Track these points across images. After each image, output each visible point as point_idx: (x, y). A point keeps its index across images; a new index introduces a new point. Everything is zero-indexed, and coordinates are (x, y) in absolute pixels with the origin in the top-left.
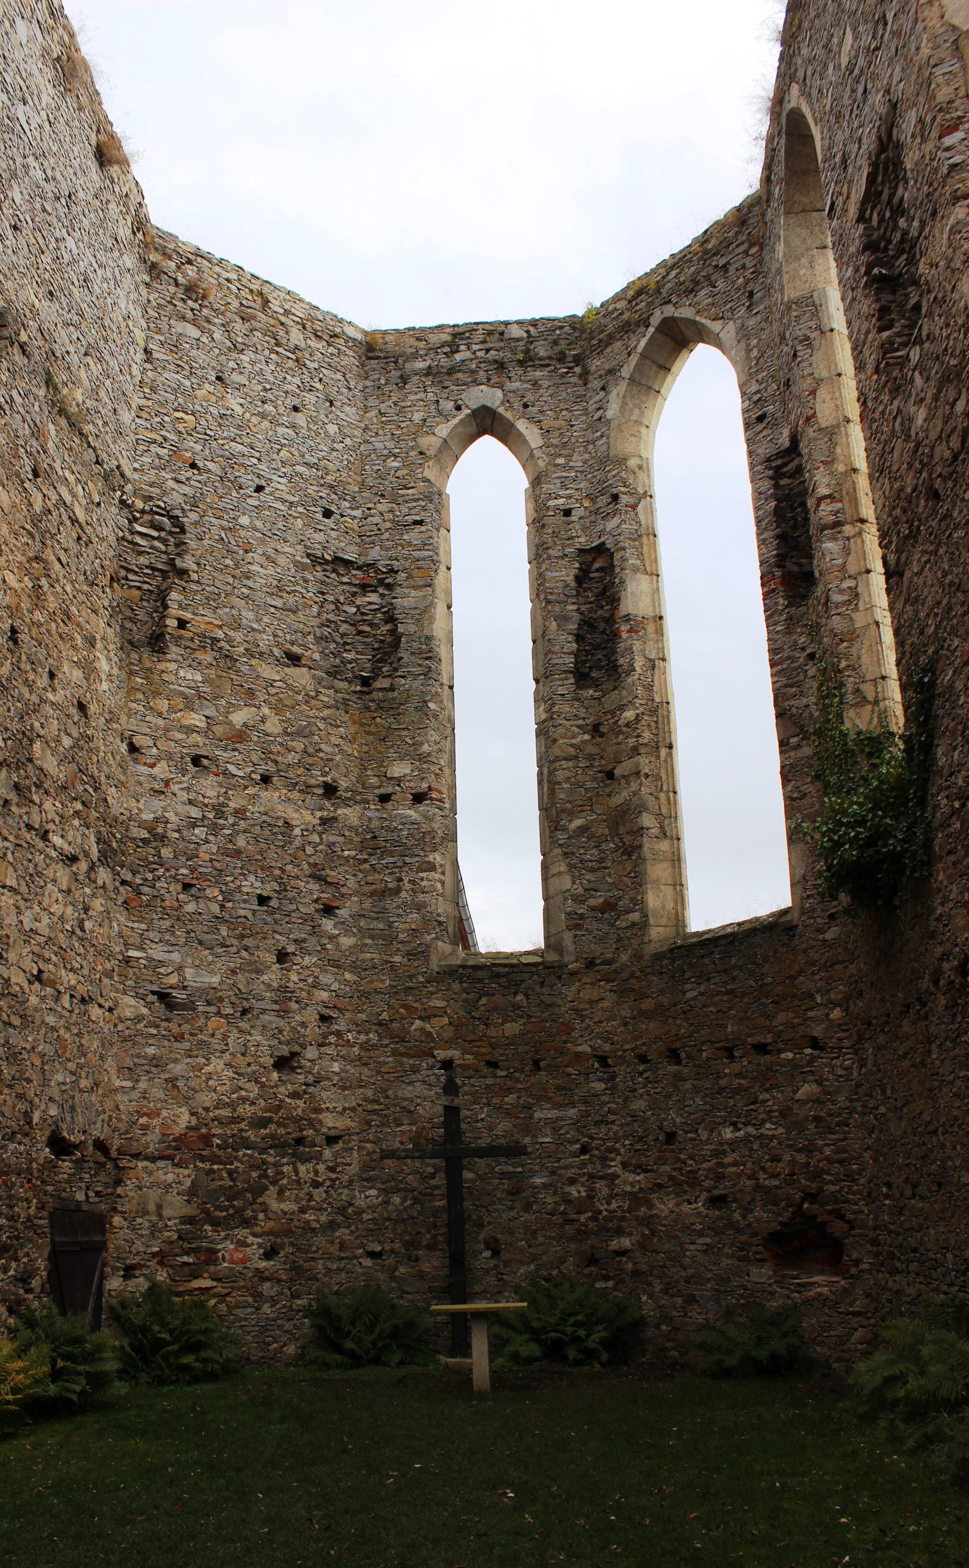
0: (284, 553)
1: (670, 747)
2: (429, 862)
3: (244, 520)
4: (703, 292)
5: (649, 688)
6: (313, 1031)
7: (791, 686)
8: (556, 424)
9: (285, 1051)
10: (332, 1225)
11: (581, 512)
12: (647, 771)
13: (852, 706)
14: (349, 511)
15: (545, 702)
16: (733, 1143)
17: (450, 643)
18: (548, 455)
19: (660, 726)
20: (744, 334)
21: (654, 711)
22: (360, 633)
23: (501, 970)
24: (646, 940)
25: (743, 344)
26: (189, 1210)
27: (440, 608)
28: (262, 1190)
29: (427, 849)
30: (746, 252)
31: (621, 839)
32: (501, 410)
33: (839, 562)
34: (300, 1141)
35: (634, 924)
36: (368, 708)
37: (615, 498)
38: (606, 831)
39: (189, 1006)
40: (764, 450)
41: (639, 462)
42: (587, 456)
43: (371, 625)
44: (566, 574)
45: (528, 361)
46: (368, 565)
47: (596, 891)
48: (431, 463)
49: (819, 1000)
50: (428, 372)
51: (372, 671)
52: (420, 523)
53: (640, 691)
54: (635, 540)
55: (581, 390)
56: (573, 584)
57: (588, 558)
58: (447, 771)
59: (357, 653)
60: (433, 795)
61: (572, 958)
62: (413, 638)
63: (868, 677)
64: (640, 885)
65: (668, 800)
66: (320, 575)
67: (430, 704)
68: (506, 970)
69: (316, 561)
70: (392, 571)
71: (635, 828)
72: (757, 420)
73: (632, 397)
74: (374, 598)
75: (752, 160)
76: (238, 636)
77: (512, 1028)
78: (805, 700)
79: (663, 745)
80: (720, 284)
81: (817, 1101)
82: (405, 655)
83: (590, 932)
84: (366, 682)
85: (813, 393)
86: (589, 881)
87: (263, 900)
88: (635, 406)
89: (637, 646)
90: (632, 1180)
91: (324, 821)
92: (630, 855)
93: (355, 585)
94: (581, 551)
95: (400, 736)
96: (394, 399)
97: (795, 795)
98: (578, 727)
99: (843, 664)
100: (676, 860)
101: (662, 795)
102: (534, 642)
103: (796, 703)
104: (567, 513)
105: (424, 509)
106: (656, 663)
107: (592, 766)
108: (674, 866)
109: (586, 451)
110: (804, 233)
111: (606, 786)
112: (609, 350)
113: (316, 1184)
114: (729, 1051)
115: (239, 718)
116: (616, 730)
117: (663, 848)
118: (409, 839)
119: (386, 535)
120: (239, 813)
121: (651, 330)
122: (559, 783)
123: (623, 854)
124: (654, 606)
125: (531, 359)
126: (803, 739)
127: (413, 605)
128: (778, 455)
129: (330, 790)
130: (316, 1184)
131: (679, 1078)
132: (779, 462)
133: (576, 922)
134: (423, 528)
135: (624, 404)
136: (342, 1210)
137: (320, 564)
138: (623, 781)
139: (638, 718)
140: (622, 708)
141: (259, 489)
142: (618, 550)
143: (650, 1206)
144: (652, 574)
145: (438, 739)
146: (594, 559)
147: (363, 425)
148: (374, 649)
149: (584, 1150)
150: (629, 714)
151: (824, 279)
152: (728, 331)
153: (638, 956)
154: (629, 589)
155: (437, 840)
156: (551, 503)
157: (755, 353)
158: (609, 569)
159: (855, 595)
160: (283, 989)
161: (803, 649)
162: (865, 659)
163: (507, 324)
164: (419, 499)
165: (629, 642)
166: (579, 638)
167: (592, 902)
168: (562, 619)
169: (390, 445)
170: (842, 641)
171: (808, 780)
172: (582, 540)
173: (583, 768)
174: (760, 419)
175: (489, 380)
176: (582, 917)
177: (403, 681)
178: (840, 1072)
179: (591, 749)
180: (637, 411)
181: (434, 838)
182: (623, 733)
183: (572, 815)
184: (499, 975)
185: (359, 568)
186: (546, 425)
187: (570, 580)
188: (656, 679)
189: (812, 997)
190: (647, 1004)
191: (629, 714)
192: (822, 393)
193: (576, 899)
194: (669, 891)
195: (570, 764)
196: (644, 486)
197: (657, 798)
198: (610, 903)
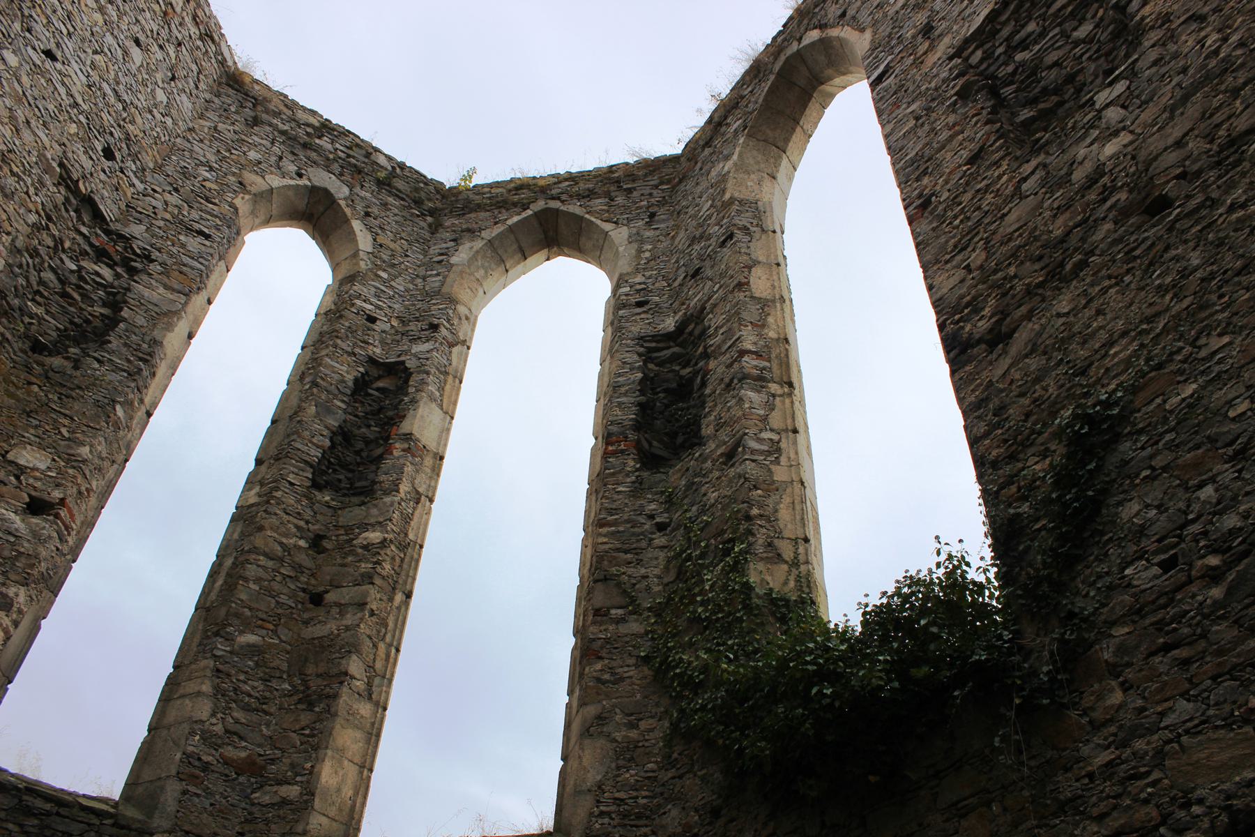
0: (35, 135)
1: (409, 595)
2: (5, 596)
5: (407, 519)
7: (626, 552)
8: (392, 245)
11: (387, 327)
12: (374, 607)
13: (762, 559)
14: (131, 175)
15: (262, 484)
17: (173, 369)
18: (373, 263)
19: (405, 566)
21: (403, 547)
22: (65, 295)
23: (39, 803)
24: (300, 828)
25: (635, 246)
27: (182, 327)
29: (13, 576)
31: (305, 682)
32: (342, 203)
35: (284, 802)
36: (29, 370)
37: (434, 327)
38: (285, 666)
41: (467, 312)
42: (411, 287)
43: (85, 296)
44: (344, 370)
45: (384, 184)
46: (121, 236)
47: (241, 738)
48: (247, 197)
51: (55, 344)
52: (207, 237)
53: (396, 515)
54: (441, 373)
55: (427, 236)
56: (351, 384)
57: (375, 372)
58: (93, 501)
59: (48, 312)
61: (166, 824)
62: (137, 330)
63: (786, 534)
64: (316, 748)
65: (388, 655)
66: (60, 199)
67: (118, 407)
68: (48, 806)
69: (66, 180)
70: (148, 258)
71: (335, 671)
73: (484, 257)
75: (699, 111)
78: (643, 571)
79: (401, 587)
80: (620, 200)
82: (115, 343)
83: (210, 794)
84: (37, 347)
86: (237, 722)
88: (483, 266)
89: (409, 469)
92: (311, 705)
93: (91, 245)
94: (372, 361)
95: (55, 421)
96: (237, 128)
97: (606, 677)
98: (297, 527)
99: (755, 511)
100: (373, 735)
101: (382, 646)
102: (274, 422)
103: (630, 571)
104: (372, 320)
105: (217, 228)
106: (422, 498)
107: (297, 579)
108: (368, 742)
109: (412, 281)
110: (760, 157)
111: (306, 610)
112: (473, 215)
116: (346, 548)
117: (363, 712)
119: (161, 223)
121: (529, 212)
122: (246, 580)
123: (300, 701)
124: (439, 444)
125: (389, 185)
126: (631, 613)
127: (155, 301)
132: (654, 345)
133: (193, 771)
134: (207, 243)
135: (473, 259)
137: (68, 187)
138: (335, 610)
139: (384, 543)
140: (365, 527)
141: (49, 54)
142: (419, 372)
144: (446, 413)
145: (104, 455)
146: (379, 378)
147: (191, 125)
148: (72, 322)
150: (374, 536)
154: (420, 410)
155: (35, 572)
156: (358, 302)
158: (402, 388)
161: (651, 517)
162: (784, 514)
163: (377, 150)
164: (216, 217)
165: (401, 461)
167: (230, 752)
169: (213, 158)
170: (756, 488)
171: (632, 661)
172: (378, 351)
173: (285, 577)
175: (341, 174)
176: (206, 767)
177: (96, 365)
179: (302, 558)
180: (482, 272)
181: (32, 566)
182: (357, 555)
183: (247, 626)
184: (29, 812)
185: (108, 232)
186: (380, 239)
187: (349, 378)
188: (417, 513)
191: (374, 536)
193: (207, 738)
194: (352, 771)
195: (270, 564)
196: (466, 335)
197: (375, 646)
198: (254, 763)
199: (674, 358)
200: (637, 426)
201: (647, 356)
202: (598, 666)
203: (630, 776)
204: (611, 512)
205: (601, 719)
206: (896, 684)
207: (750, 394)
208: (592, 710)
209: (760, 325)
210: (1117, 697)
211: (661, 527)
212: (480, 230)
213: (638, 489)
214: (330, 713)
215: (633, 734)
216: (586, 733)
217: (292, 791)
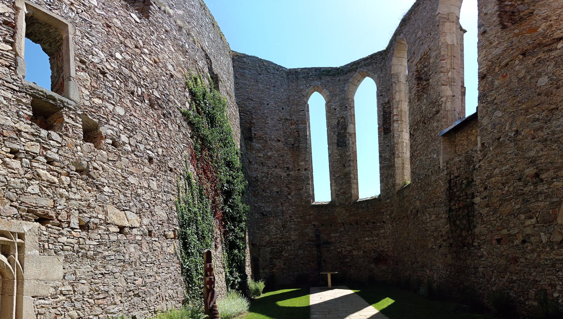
3: (266, 111)
5: (353, 148)
6: (289, 219)
9: (284, 223)
10: (294, 258)
16: (368, 241)
26: (270, 257)
28: (281, 252)
34: (288, 242)
37: (346, 107)
39: (266, 215)
40: (381, 102)
44: (335, 122)
50: (303, 77)
60: (309, 169)
72: (380, 95)
74: (293, 127)
76: (267, 136)
77: (326, 217)
80: (375, 66)
81: (384, 233)
84: (293, 145)
87: (277, 192)
89: (350, 139)
90: (349, 248)
91: (287, 175)
113: (291, 250)
114: (367, 223)
115: (269, 154)
116: (345, 156)
118: (305, 179)
120: (271, 174)
129: (288, 168)
130: (291, 250)
131: (358, 228)
133: (337, 196)
136: (296, 255)
143: (352, 252)
149: (340, 242)
151: (402, 68)
153: (350, 203)
160: (282, 210)
162: (400, 148)
166: (338, 136)
168: (334, 132)
174: (381, 95)
190: (352, 213)
191: (349, 154)
192: (397, 94)
200: (383, 124)
206: (240, 280)
212: (348, 79)
214: (350, 183)
217: (349, 195)
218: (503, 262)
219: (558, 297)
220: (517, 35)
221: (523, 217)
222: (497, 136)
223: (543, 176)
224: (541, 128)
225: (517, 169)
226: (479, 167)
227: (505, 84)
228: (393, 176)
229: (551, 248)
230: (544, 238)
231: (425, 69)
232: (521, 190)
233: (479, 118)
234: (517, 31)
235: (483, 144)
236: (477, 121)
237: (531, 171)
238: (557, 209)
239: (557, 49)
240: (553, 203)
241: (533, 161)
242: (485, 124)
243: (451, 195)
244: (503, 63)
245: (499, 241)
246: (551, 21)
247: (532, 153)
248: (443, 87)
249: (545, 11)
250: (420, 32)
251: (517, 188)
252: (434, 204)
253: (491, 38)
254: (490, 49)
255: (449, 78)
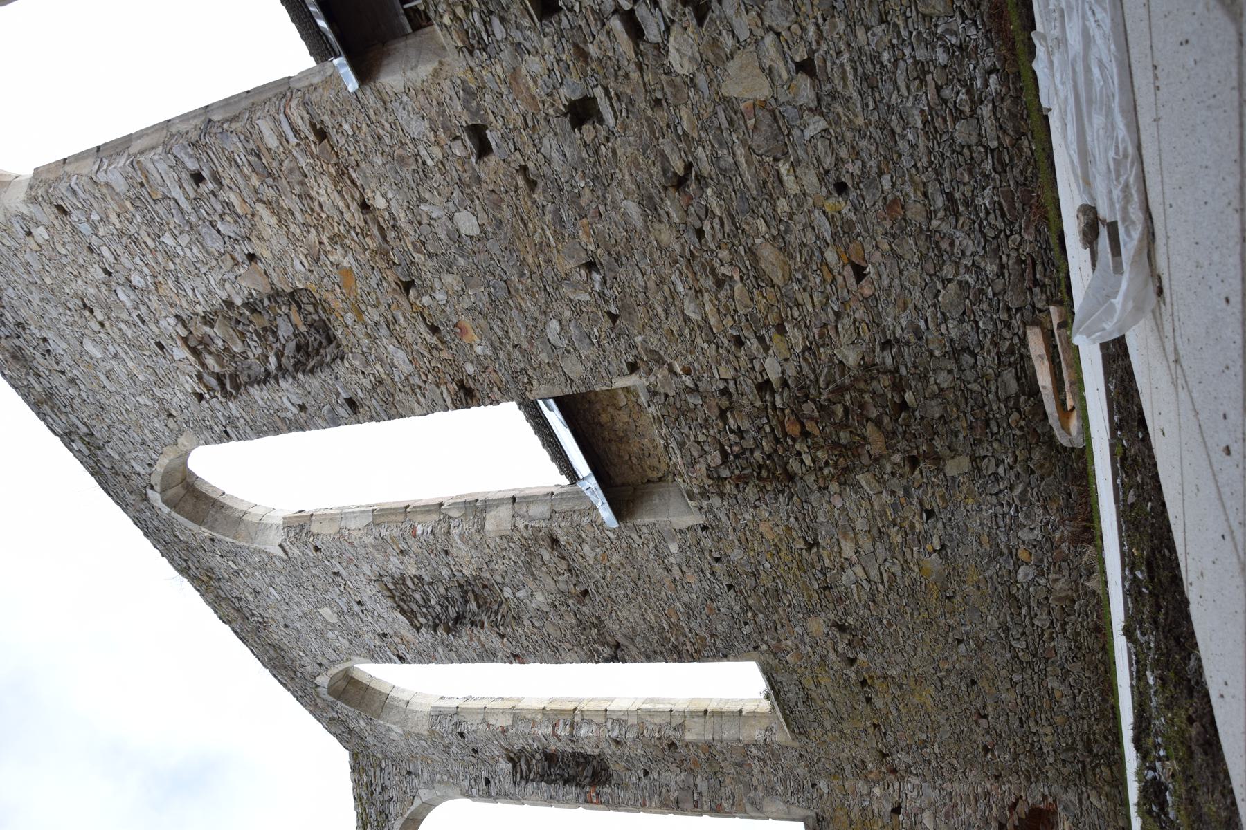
4: (392, 808)
20: (430, 784)
25: (436, 785)
30: (382, 770)
33: (595, 727)
49: (866, 803)
80: (393, 794)
85: (489, 725)
128: (514, 775)
151: (426, 685)
152: (425, 794)
157: (445, 778)
159: (617, 721)
162: (657, 720)
174: (488, 782)
178: (915, 793)
189: (864, 809)
192: (491, 721)
199: (528, 763)
200: (578, 785)
201: (526, 779)
202: (725, 805)
203: (780, 789)
204: (636, 800)
205: (753, 803)
207: (583, 732)
208: (748, 807)
209: (533, 723)
210: (789, 643)
211: (646, 773)
213: (621, 785)
215: (760, 788)
216: (760, 809)
218: (909, 247)
219: (947, 50)
220: (360, 313)
221: (782, 204)
222: (606, 324)
223: (678, 166)
224: (575, 199)
225: (677, 248)
226: (687, 372)
227: (483, 322)
228: (743, 755)
229: (834, 99)
230: (816, 125)
231: (433, 602)
232: (722, 224)
233: (568, 391)
234: (350, 318)
235: (633, 368)
236: (583, 396)
237: (671, 205)
238: (742, 106)
239: (388, 209)
240: (731, 122)
241: (650, 206)
242: (580, 368)
243: (777, 476)
244: (433, 340)
245: (859, 273)
246: (321, 243)
247: (633, 209)
248: (487, 527)
249: (297, 263)
250: (326, 612)
251: (719, 235)
252: (810, 547)
253: (366, 382)
254: (395, 383)
255: (465, 515)
